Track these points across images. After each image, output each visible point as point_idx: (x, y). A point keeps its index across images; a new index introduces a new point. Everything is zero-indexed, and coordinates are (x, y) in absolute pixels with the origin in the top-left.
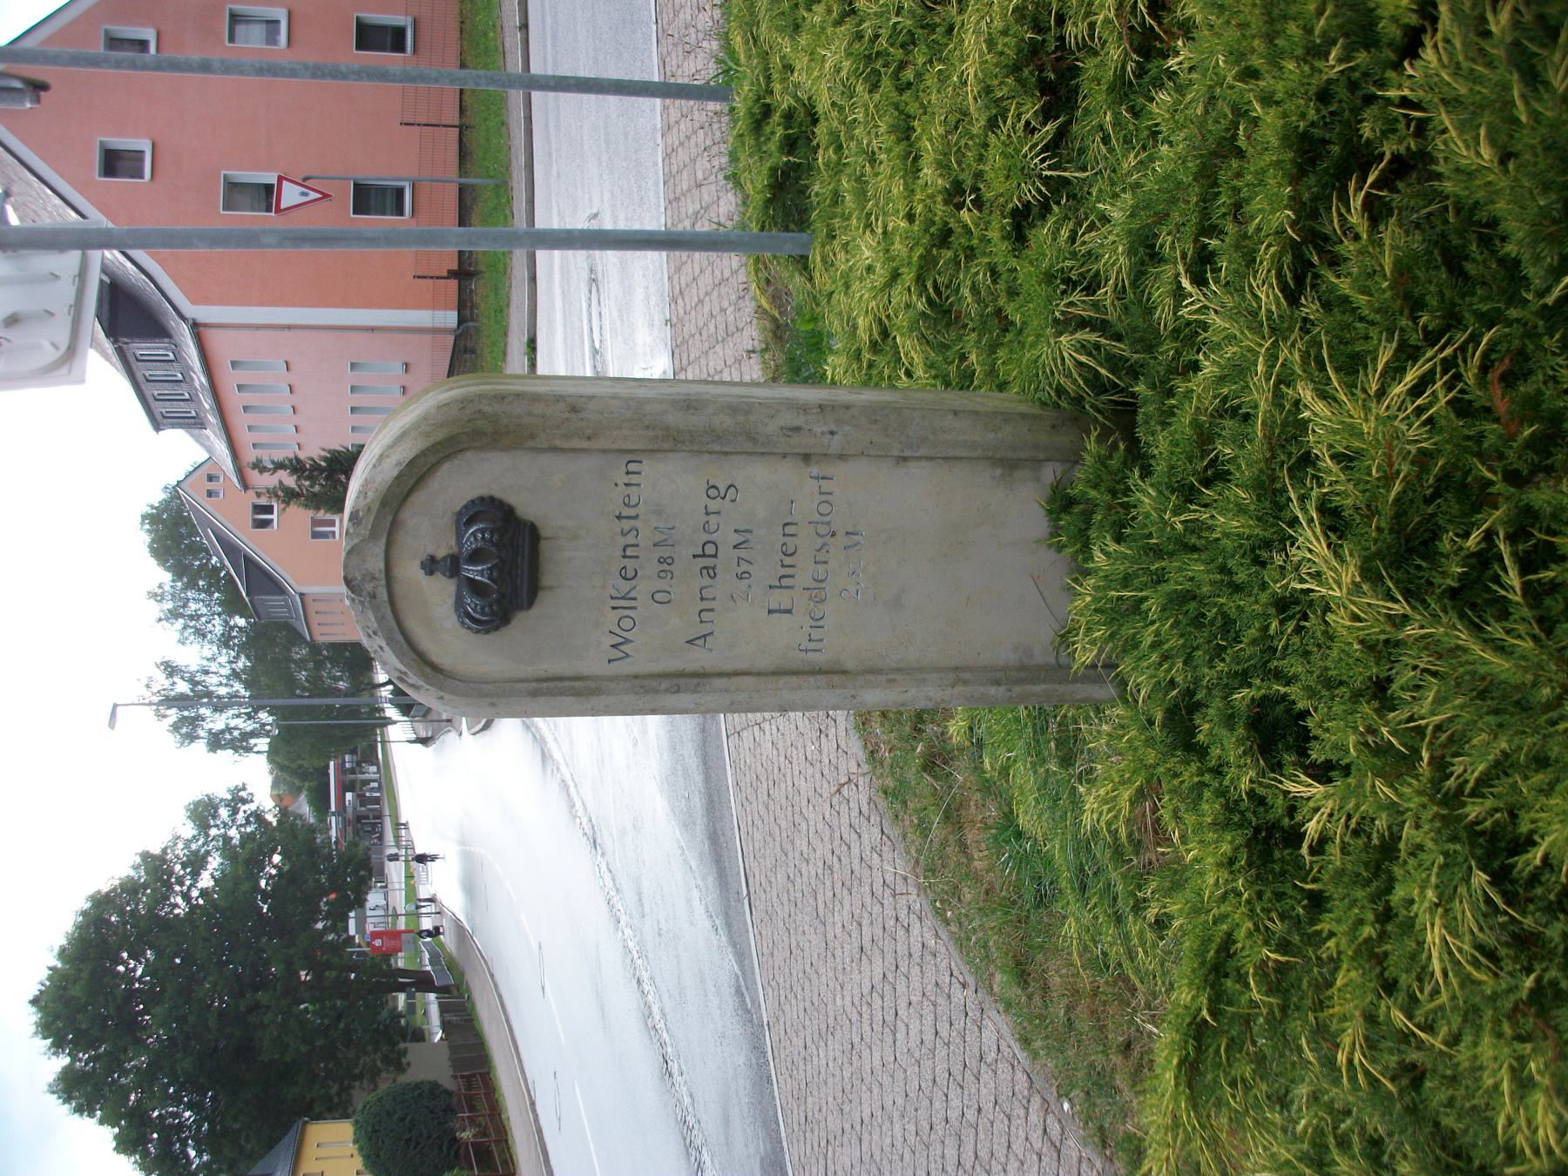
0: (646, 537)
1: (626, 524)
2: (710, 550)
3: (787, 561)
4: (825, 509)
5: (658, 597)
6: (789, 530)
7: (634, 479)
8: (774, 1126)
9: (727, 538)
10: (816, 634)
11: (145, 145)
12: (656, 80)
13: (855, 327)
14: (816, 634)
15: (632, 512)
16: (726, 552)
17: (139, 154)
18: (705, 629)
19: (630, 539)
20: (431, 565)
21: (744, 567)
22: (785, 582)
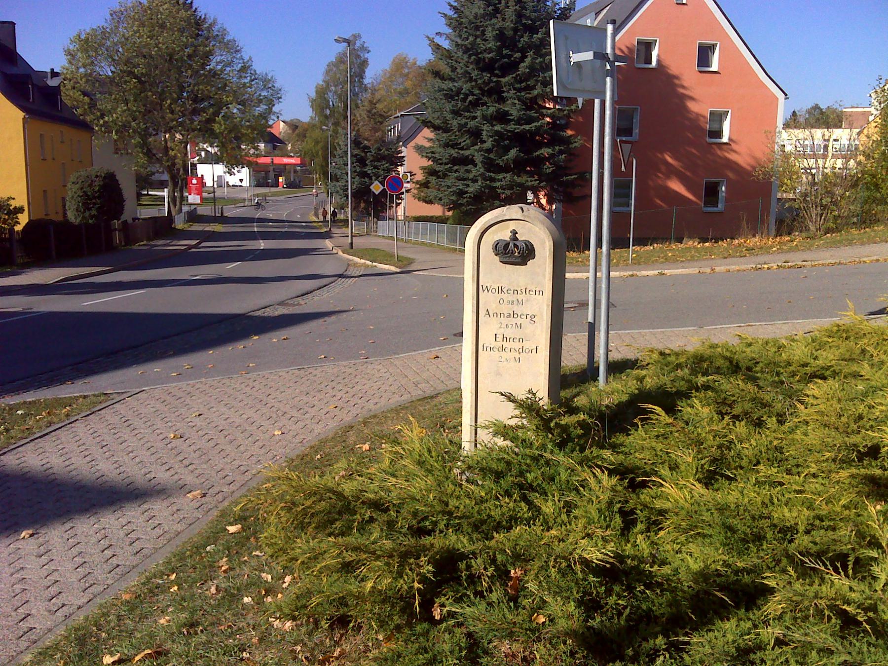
0: (520, 297)
1: (524, 291)
2: (515, 316)
3: (511, 340)
4: (527, 351)
5: (502, 301)
6: (521, 340)
7: (537, 293)
8: (352, 67)
9: (519, 321)
10: (488, 349)
11: (721, 206)
12: (567, 275)
13: (849, 604)
14: (488, 349)
15: (527, 292)
16: (514, 321)
17: (715, 204)
18: (491, 315)
19: (519, 292)
20: (514, 233)
21: (510, 326)
22: (505, 339)
